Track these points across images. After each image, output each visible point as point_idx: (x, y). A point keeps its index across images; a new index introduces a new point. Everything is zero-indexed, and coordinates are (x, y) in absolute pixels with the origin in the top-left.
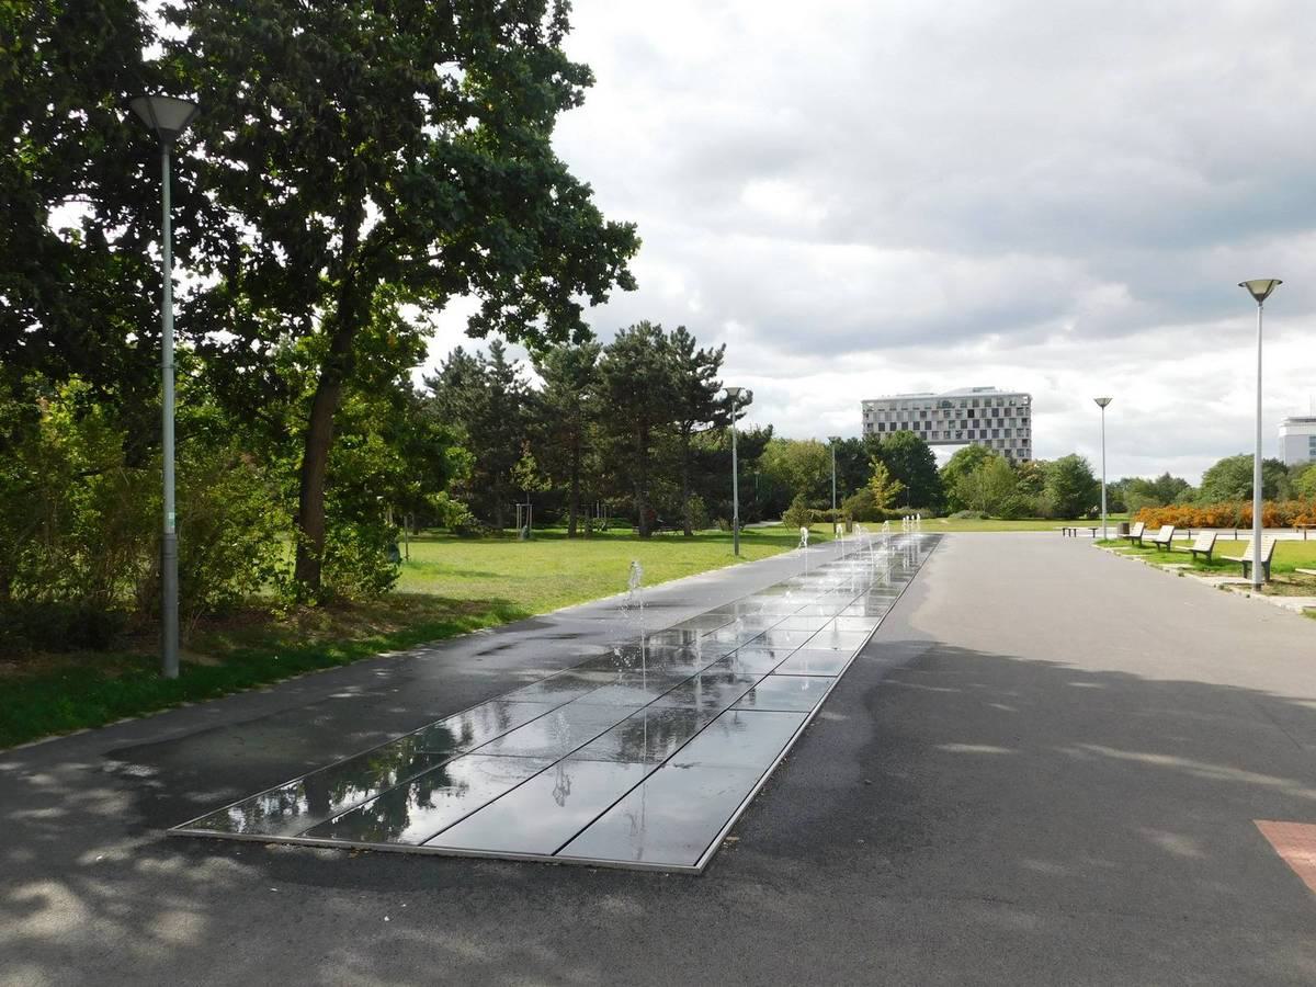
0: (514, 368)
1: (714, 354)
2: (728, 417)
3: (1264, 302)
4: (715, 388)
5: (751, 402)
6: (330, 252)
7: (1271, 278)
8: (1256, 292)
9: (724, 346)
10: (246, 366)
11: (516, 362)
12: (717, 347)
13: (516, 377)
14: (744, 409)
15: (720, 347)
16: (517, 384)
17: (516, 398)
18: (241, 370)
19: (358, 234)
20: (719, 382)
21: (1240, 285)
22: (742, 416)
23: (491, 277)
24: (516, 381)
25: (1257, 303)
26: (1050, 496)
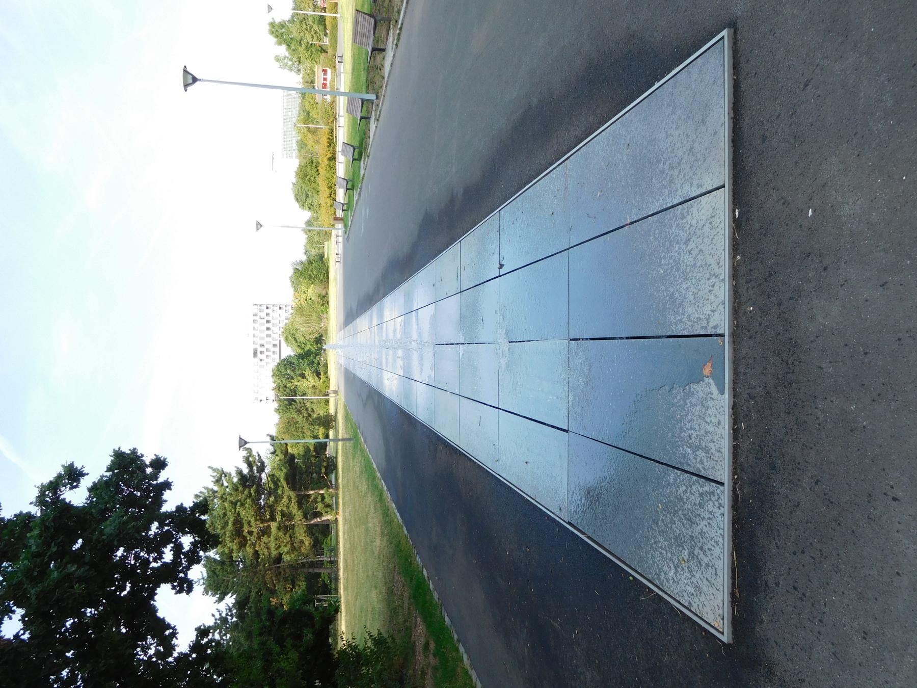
0: (218, 616)
1: (215, 474)
2: (259, 464)
3: (198, 77)
4: (240, 473)
5: (251, 449)
6: (217, 586)
7: (183, 71)
8: (191, 81)
9: (209, 467)
10: (187, 587)
11: (213, 615)
12: (210, 472)
13: (224, 615)
14: (254, 453)
15: (210, 470)
16: (229, 614)
17: (240, 616)
18: (185, 586)
19: (168, 658)
20: (236, 469)
21: (186, 91)
22: (259, 455)
23: (576, 650)
24: (227, 615)
25: (198, 83)
26: (312, 291)
